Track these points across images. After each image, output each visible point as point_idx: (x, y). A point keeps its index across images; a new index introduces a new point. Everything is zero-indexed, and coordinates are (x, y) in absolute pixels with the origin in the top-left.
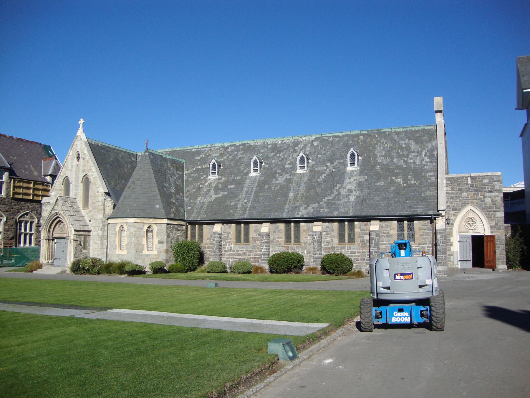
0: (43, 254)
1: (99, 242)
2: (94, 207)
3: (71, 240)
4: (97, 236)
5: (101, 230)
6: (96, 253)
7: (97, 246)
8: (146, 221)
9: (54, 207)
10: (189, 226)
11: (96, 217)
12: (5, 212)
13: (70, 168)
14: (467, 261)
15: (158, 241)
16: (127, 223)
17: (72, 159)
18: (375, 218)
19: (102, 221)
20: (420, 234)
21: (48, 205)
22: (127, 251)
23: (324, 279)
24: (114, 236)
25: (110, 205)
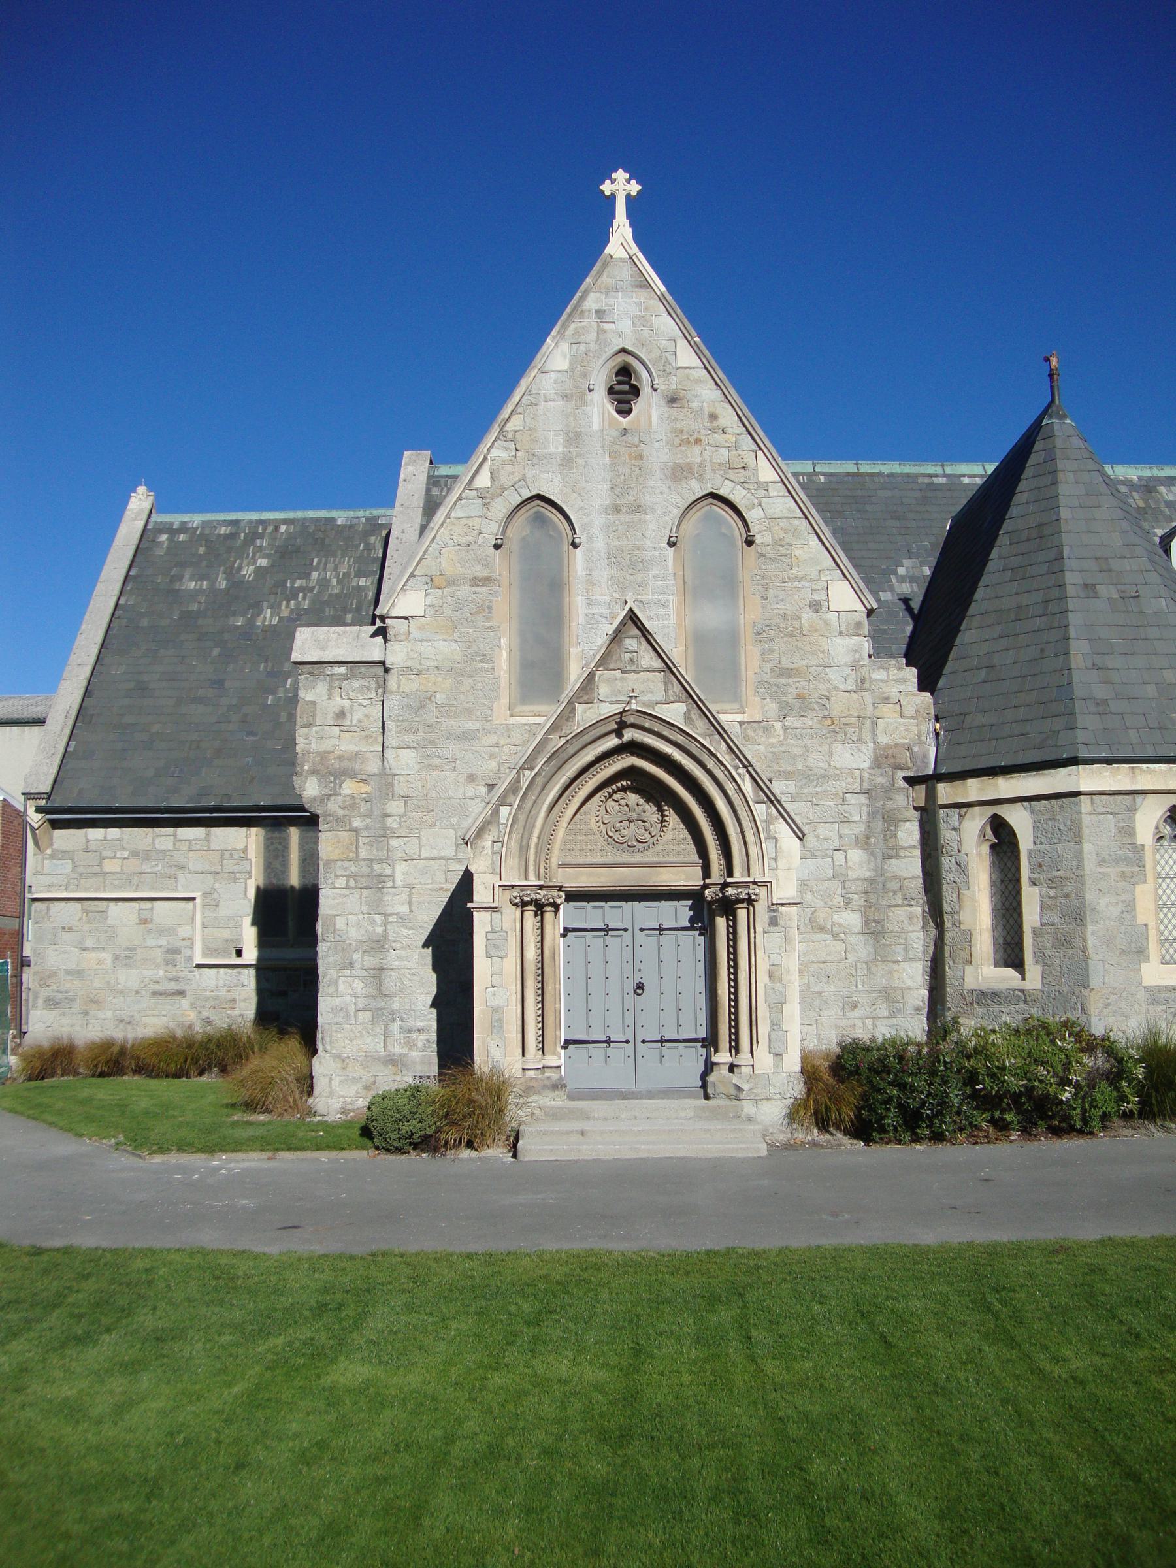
0: (496, 1010)
1: (852, 919)
2: (791, 699)
3: (773, 907)
4: (836, 885)
5: (864, 843)
6: (830, 989)
7: (839, 947)
9: (591, 676)
11: (816, 763)
13: (557, 446)
14: (662, 1041)
17: (576, 396)
19: (867, 791)
21: (346, 678)
25: (909, 693)
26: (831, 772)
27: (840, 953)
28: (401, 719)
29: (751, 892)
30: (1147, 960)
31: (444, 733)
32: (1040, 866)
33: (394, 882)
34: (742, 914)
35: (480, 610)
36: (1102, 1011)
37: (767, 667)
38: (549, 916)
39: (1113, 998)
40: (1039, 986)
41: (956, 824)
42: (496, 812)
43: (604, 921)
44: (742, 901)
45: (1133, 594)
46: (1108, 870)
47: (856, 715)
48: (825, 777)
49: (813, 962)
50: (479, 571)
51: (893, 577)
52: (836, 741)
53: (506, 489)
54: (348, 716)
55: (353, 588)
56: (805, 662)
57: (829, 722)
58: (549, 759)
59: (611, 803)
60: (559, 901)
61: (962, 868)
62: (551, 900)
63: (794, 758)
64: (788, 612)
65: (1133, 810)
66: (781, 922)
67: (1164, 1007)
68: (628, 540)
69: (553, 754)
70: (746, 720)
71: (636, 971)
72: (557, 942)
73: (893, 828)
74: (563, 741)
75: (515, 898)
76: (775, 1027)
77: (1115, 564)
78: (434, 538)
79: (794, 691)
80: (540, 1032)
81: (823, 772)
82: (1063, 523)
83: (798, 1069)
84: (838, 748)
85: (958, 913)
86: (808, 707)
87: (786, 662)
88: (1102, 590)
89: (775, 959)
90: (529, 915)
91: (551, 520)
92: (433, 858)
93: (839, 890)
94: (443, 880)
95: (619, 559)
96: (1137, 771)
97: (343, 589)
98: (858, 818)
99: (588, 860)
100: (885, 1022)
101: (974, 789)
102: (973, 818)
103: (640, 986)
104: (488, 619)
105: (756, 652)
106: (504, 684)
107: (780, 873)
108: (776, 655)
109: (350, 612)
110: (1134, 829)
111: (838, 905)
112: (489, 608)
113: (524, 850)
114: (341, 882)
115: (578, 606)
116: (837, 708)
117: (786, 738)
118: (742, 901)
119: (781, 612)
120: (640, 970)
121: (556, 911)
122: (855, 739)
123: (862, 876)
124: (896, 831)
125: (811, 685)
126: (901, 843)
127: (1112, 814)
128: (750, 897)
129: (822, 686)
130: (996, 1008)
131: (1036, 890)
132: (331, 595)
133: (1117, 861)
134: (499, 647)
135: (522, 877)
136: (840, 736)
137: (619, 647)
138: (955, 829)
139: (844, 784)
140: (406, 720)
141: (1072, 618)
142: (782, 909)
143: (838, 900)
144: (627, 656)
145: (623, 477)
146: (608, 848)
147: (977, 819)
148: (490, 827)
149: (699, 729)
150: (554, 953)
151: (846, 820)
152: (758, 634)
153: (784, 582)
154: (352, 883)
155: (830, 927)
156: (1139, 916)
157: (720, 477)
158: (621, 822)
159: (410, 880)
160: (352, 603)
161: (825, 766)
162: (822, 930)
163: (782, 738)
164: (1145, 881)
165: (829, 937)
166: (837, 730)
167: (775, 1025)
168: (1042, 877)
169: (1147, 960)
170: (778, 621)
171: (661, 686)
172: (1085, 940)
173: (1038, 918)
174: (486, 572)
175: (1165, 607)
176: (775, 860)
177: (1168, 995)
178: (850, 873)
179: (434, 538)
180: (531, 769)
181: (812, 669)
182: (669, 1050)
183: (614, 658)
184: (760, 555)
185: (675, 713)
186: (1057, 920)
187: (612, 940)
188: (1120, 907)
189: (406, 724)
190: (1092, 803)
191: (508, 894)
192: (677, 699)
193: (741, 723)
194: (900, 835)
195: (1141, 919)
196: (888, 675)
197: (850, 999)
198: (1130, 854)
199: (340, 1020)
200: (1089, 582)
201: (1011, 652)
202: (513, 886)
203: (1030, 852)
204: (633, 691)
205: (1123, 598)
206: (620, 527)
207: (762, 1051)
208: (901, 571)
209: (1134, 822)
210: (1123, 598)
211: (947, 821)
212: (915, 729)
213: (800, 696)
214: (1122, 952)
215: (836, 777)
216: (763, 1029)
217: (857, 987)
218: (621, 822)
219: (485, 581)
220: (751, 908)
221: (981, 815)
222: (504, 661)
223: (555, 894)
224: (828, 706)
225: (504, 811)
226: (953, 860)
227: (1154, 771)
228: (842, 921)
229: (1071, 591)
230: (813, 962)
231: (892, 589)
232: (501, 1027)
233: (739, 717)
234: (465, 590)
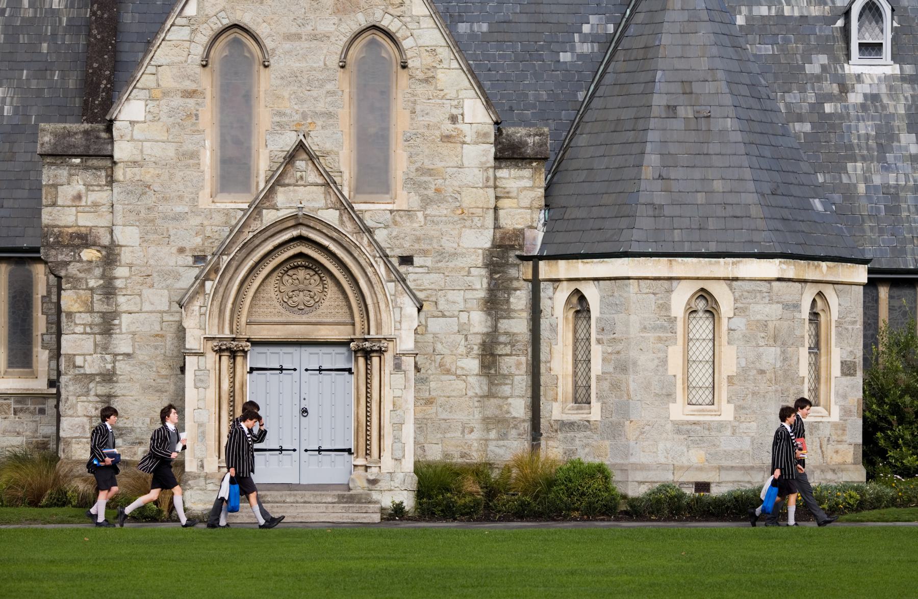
0: (200, 425)
1: (473, 365)
2: (430, 193)
3: (397, 357)
4: (460, 338)
7: (461, 385)
8: (811, 271)
10: (884, 292)
12: (422, 237)
15: (842, 363)
16: (736, 279)
18: (76, 156)
20: (195, 256)
22: (738, 408)
23: (870, 518)
24: (660, 339)
26: (459, 250)
27: (461, 390)
28: (126, 202)
29: (381, 345)
30: (675, 401)
31: (161, 215)
32: (603, 330)
33: (121, 329)
34: (375, 360)
35: (189, 116)
36: (637, 438)
37: (413, 168)
38: (239, 360)
39: (647, 428)
40: (599, 418)
41: (551, 294)
42: (203, 285)
43: (279, 362)
44: (376, 351)
45: (705, 115)
46: (649, 334)
47: (481, 206)
48: (455, 255)
49: (440, 396)
50: (189, 85)
51: (576, 36)
52: (465, 227)
53: (210, 18)
54: (84, 199)
55: (46, 12)
56: (443, 164)
57: (460, 212)
58: (240, 248)
59: (286, 278)
60: (246, 349)
61: (554, 329)
62: (241, 348)
63: (431, 239)
64: (431, 123)
65: (670, 291)
66: (403, 367)
67: (685, 436)
68: (307, 62)
69: (244, 245)
70: (395, 209)
71: (302, 399)
72: (245, 378)
73: (506, 295)
74: (251, 235)
75: (215, 346)
76: (396, 441)
77: (696, 87)
78: (152, 57)
79: (433, 187)
80: (232, 384)
81: (453, 250)
82: (661, 50)
83: (412, 470)
84: (467, 233)
85: (549, 362)
86: (444, 200)
87: (428, 164)
88: (681, 111)
89: (398, 393)
90: (225, 359)
91: (246, 45)
92: (151, 312)
93: (463, 342)
94: (159, 329)
95: (300, 78)
96: (674, 263)
97: (36, 12)
98: (478, 287)
99: (269, 319)
100: (494, 443)
101: (563, 269)
102: (562, 291)
103: (305, 411)
104: (194, 124)
105: (405, 155)
106: (207, 176)
107: (403, 332)
108: (420, 157)
109: (45, 41)
110: (669, 305)
111: (460, 353)
112: (197, 115)
113: (221, 312)
114: (79, 329)
115: (263, 117)
116: (467, 200)
117: (425, 224)
118: (376, 351)
119: (426, 123)
120: (304, 399)
121: (245, 357)
122: (479, 225)
123: (480, 331)
124: (509, 297)
125: (447, 182)
126: (512, 307)
127: (653, 294)
128: (381, 348)
129: (455, 183)
130: (572, 434)
131: (600, 346)
132: (23, 18)
133: (654, 329)
134: (204, 147)
135: (221, 331)
136: (468, 223)
137: (293, 167)
138: (550, 298)
139: (469, 261)
140: (130, 204)
141: (652, 136)
142: (404, 358)
143: (462, 350)
144: (299, 174)
145: (303, 10)
146: (283, 311)
147: (565, 291)
148: (198, 296)
149: (348, 229)
150: (243, 385)
151: (470, 288)
152: (406, 141)
153: (429, 99)
154: (88, 330)
155: (454, 370)
156: (669, 369)
157: (381, 11)
158: (293, 291)
159: (133, 328)
160: (46, 29)
161: (455, 245)
162: (448, 372)
163: (422, 223)
164: (676, 344)
165: (454, 377)
166: (466, 218)
167: (397, 439)
168: (605, 337)
169: (675, 401)
170: (423, 130)
171: (322, 196)
172: (628, 385)
173: (600, 368)
174: (193, 86)
175: (729, 126)
176: (400, 323)
177: (689, 427)
178: (471, 329)
179: (152, 57)
180: (228, 255)
181: (448, 170)
182: (326, 457)
183: (289, 175)
184: (411, 77)
185: (331, 216)
186: (611, 370)
187: (284, 376)
188: (656, 362)
189: (130, 207)
190: (639, 286)
191: (210, 344)
192: (333, 206)
193: (391, 211)
194: (512, 300)
195: (671, 372)
196: (510, 174)
197: (468, 426)
198: (666, 324)
199: (78, 435)
200: (672, 103)
201: (606, 158)
202: (214, 338)
203: (598, 320)
204: (301, 203)
205: (696, 118)
206: (301, 52)
207: (386, 455)
208: (586, 28)
209: (670, 300)
210: (696, 118)
211: (546, 290)
212: (528, 217)
213: (437, 191)
214: (656, 395)
215: (463, 255)
216: (387, 442)
217: (474, 416)
218: (293, 291)
219: (189, 94)
220: (382, 357)
221: (568, 289)
222: (208, 159)
223: (244, 344)
224: (459, 199)
225: (208, 284)
226: (548, 322)
227: (687, 263)
228: (463, 365)
229: (655, 111)
230: (440, 396)
231: (572, 50)
232: (204, 437)
233: (390, 207)
234: (177, 101)
